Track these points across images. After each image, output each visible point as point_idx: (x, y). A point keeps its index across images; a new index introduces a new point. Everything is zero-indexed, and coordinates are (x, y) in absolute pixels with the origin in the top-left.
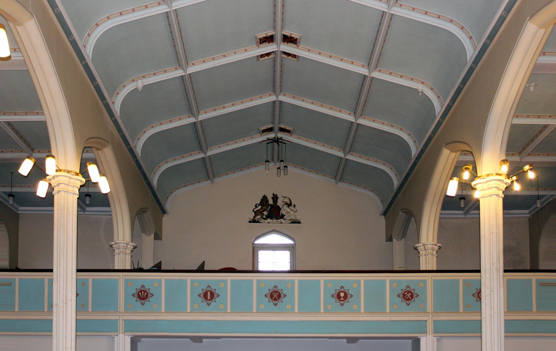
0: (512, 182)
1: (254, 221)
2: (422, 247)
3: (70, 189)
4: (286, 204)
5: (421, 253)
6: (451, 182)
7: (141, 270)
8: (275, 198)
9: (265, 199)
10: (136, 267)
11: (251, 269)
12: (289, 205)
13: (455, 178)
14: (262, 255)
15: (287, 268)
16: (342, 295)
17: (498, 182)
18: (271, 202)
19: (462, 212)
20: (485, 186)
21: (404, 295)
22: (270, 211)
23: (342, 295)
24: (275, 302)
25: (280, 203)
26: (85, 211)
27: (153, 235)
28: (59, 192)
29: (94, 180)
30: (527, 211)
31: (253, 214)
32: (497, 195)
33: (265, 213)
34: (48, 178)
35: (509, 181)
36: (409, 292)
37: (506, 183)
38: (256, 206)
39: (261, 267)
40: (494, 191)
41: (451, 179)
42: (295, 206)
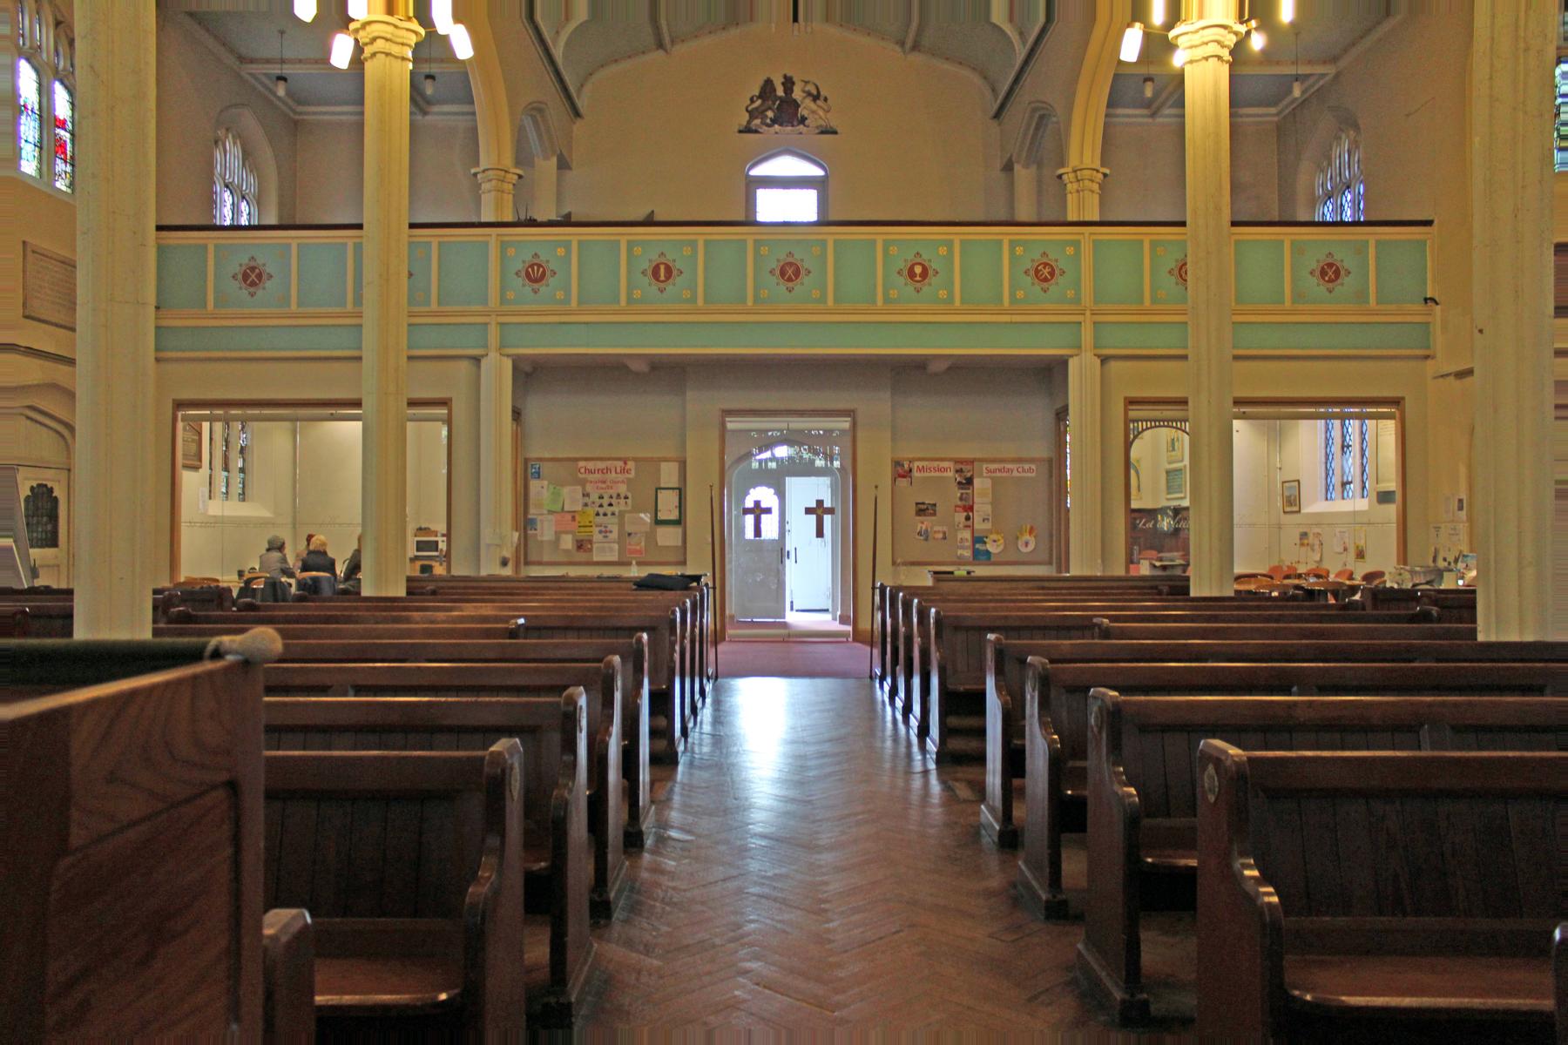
0: (1248, 33)
1: (747, 130)
2: (1072, 176)
3: (395, 50)
4: (809, 94)
5: (1069, 186)
6: (1129, 31)
7: (532, 223)
8: (789, 83)
9: (768, 85)
10: (523, 218)
11: (741, 218)
12: (816, 98)
13: (1138, 25)
14: (764, 197)
15: (813, 217)
16: (918, 270)
17: (1221, 31)
18: (780, 92)
19: (1145, 112)
20: (1196, 39)
21: (1037, 271)
22: (779, 110)
23: (918, 270)
24: (790, 285)
25: (797, 94)
26: (425, 113)
27: (554, 160)
28: (374, 55)
29: (441, 30)
30: (1273, 110)
31: (747, 116)
32: (1219, 58)
33: (770, 114)
34: (352, 26)
35: (1243, 29)
36: (1046, 264)
37: (1236, 33)
38: (752, 101)
39: (760, 218)
40: (1213, 49)
41: (1129, 26)
42: (826, 99)
